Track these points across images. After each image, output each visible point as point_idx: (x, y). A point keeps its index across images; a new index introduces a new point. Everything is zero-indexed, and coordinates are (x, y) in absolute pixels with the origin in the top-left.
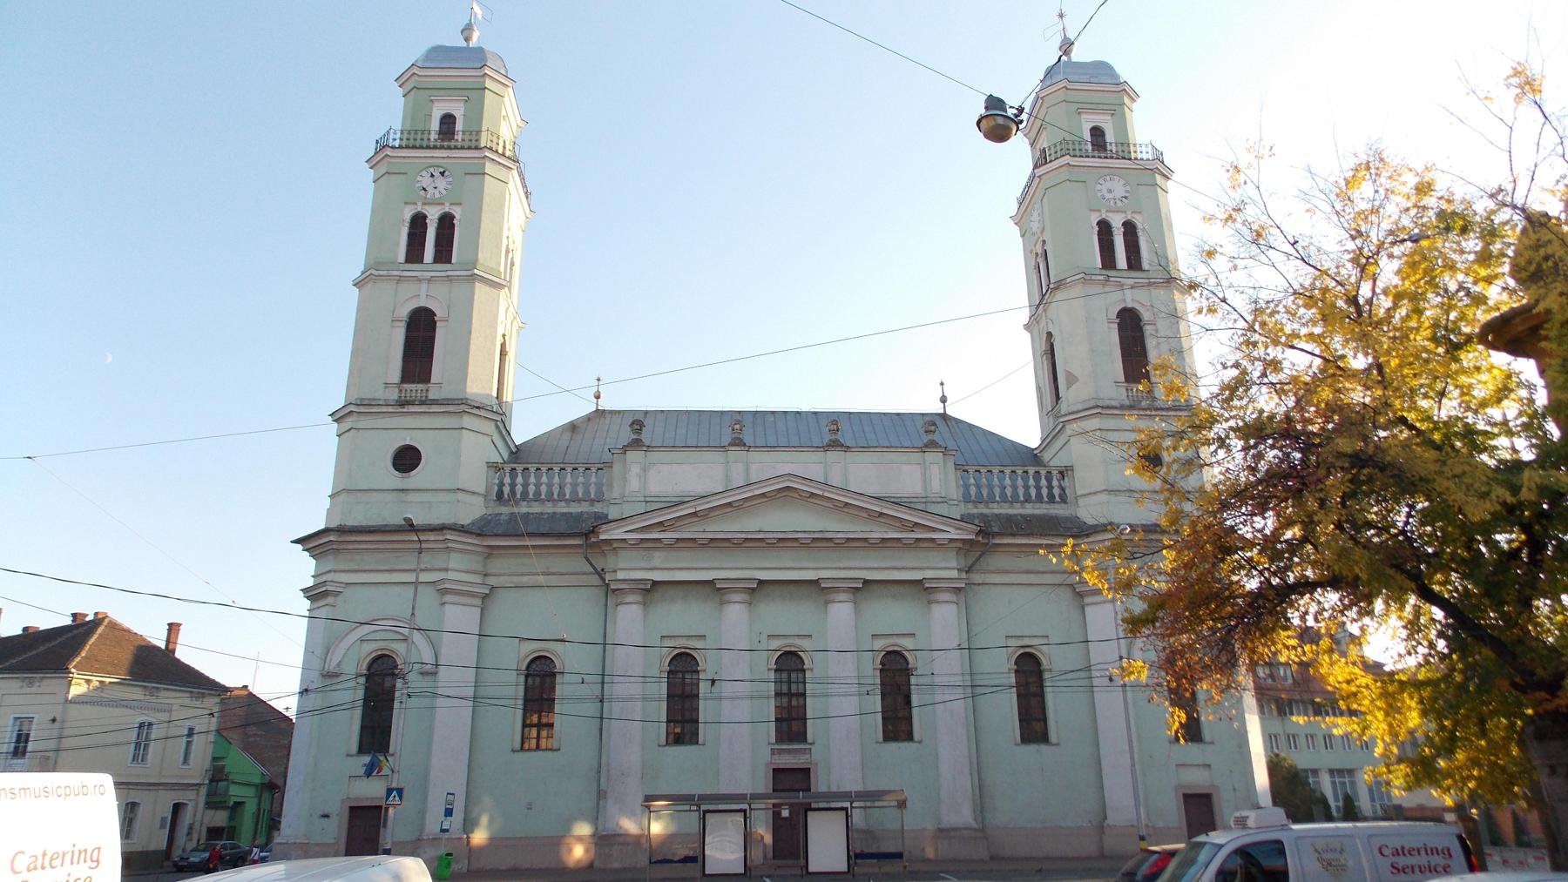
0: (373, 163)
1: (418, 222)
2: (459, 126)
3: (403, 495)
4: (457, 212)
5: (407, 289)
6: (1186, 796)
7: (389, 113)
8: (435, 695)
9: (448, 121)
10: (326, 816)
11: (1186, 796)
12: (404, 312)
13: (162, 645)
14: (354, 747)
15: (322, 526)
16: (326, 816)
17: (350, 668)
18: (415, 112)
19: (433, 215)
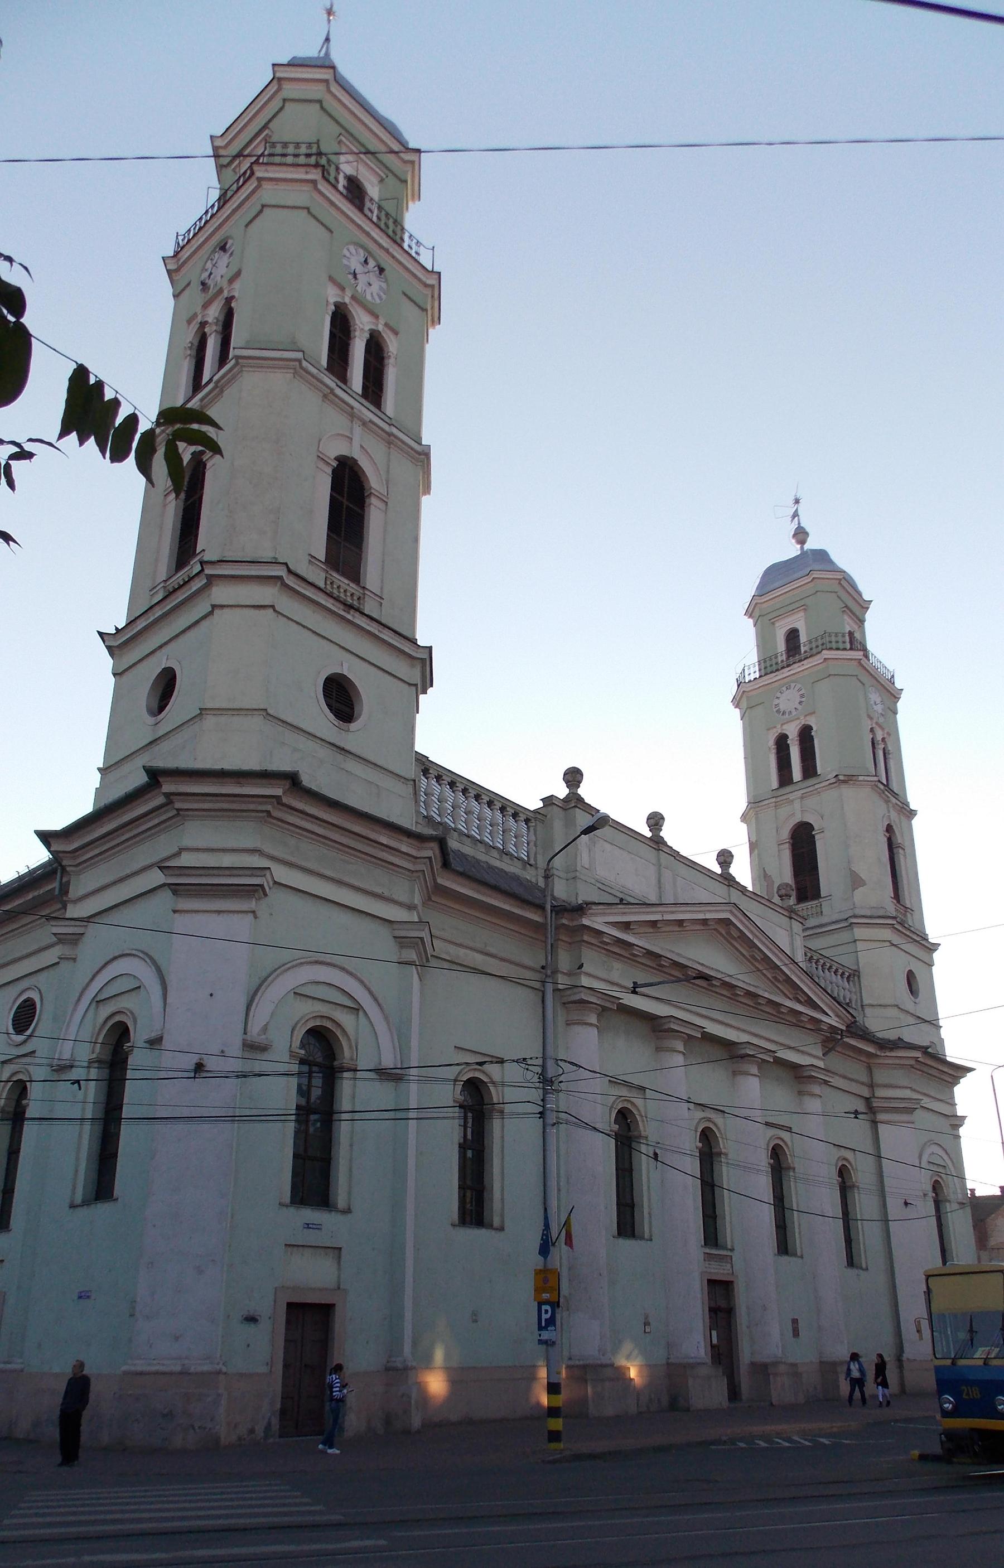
0: (737, 702)
1: (782, 743)
2: (803, 638)
3: (340, 757)
4: (812, 721)
5: (784, 811)
6: (709, 1281)
7: (740, 650)
8: (355, 1070)
9: (792, 636)
10: (251, 1319)
11: (709, 1281)
12: (786, 834)
13: (27, 1116)
14: (287, 1198)
15: (85, 807)
16: (251, 1319)
17: (85, 1053)
18: (764, 641)
19: (792, 731)
